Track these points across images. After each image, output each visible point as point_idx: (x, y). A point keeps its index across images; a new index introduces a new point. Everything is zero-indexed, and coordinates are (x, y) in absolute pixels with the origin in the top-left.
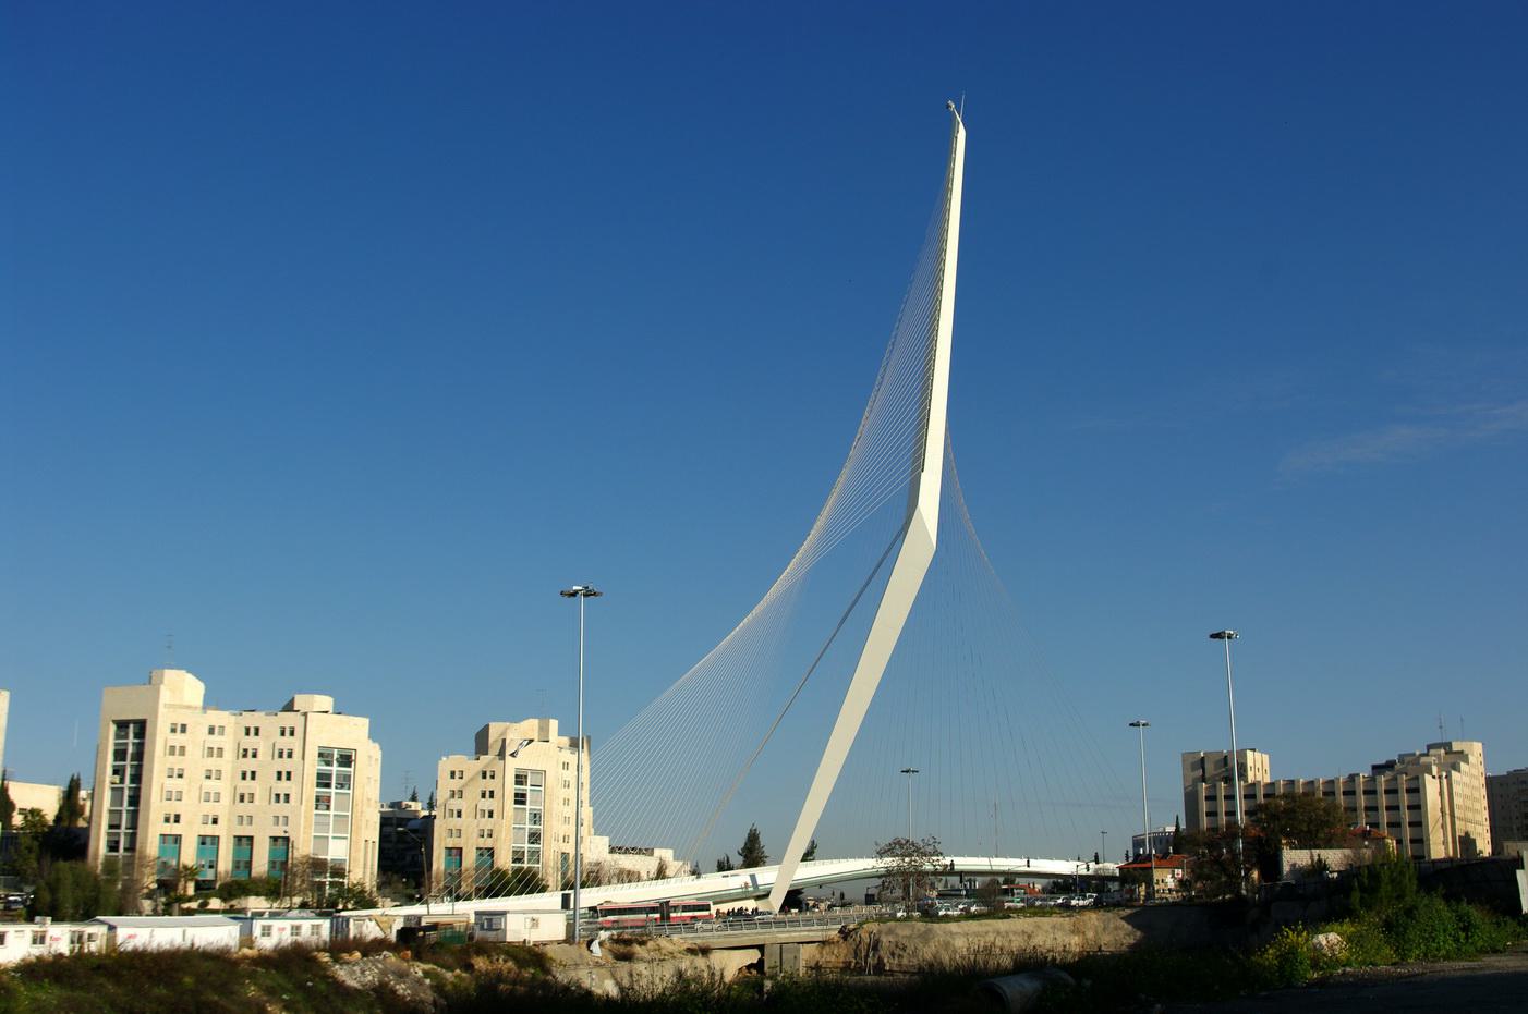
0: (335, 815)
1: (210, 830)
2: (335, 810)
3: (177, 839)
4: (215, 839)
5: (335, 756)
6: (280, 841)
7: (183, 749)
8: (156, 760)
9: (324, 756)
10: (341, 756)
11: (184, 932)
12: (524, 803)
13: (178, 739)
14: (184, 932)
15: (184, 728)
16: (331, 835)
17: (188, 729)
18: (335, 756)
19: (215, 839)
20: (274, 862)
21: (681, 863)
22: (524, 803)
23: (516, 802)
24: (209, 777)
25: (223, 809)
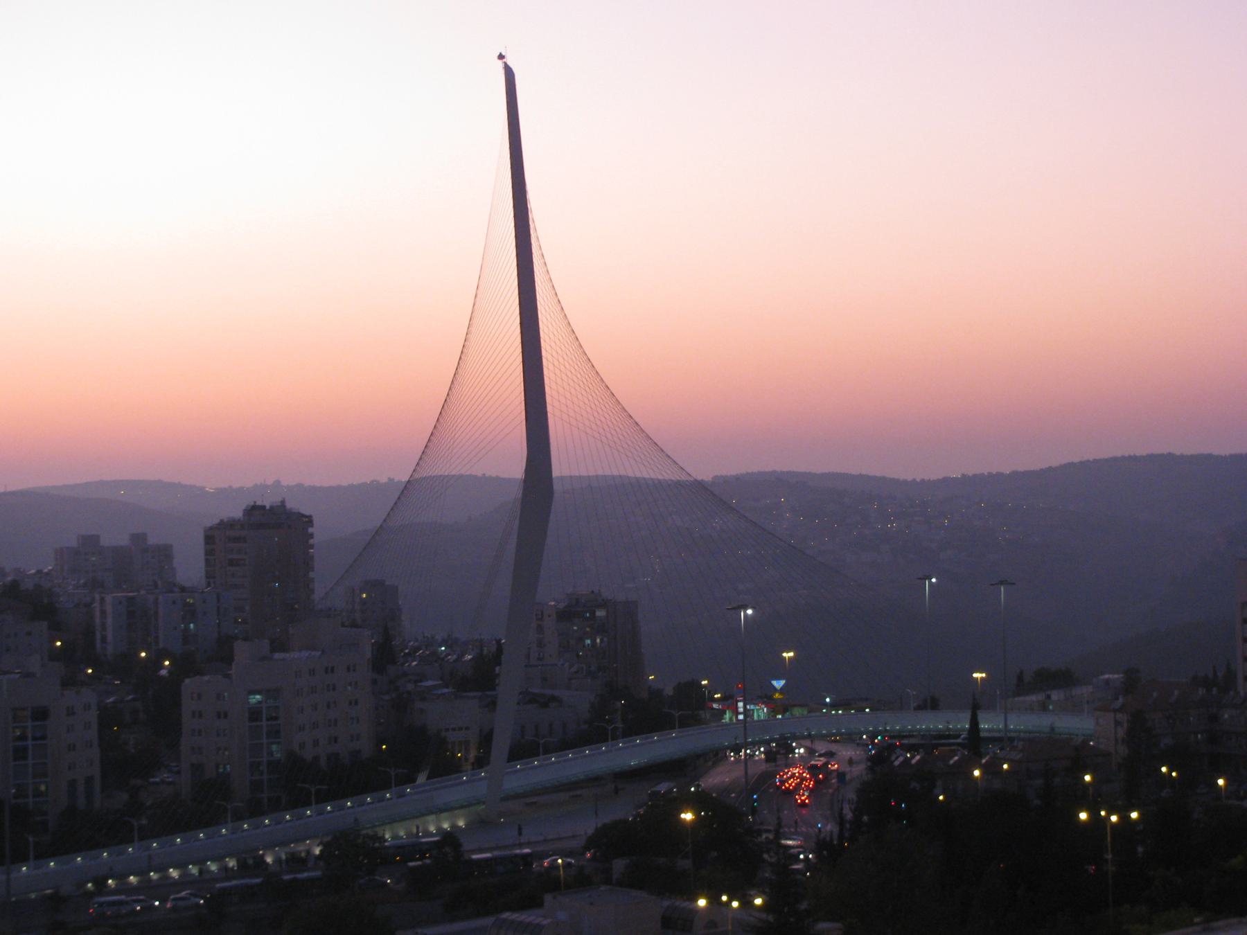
22: (25, 758)
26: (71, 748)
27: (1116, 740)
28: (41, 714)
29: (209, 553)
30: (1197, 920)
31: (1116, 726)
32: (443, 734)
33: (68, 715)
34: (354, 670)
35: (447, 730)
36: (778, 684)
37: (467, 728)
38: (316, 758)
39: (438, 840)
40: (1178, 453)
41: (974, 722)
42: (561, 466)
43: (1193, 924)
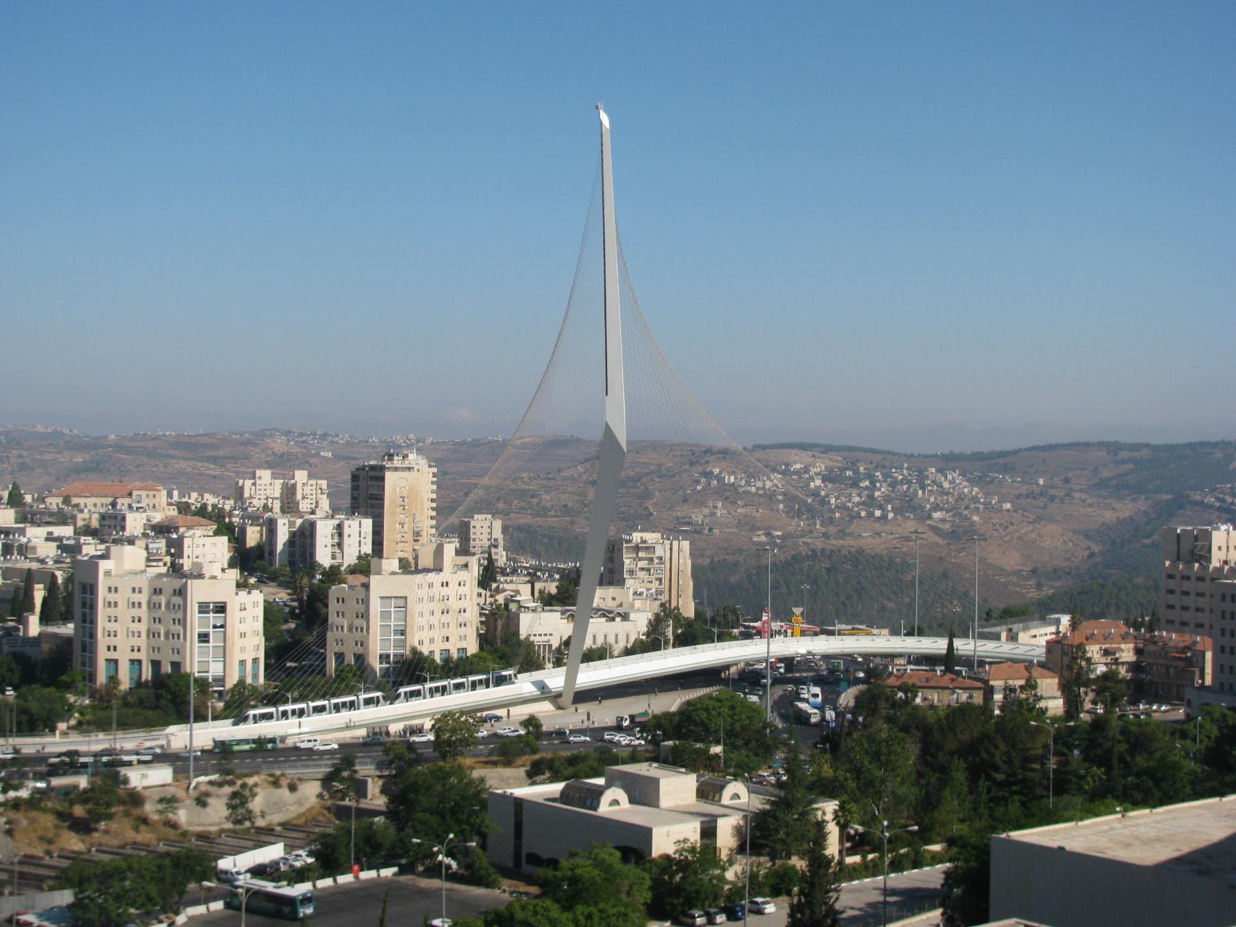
0: (213, 647)
1: (136, 656)
2: (214, 642)
3: (116, 661)
4: (140, 662)
5: (211, 607)
6: (136, 663)
7: (116, 604)
8: (877, 646)
9: (204, 608)
10: (217, 607)
11: (509, 711)
12: (208, 641)
13: (112, 597)
14: (509, 711)
15: (116, 590)
16: (211, 659)
17: (119, 590)
18: (211, 607)
19: (140, 662)
20: (1222, 666)
21: (124, 771)
22: (208, 641)
23: (200, 641)
24: (133, 621)
25: (142, 641)
26: (243, 635)
27: (1062, 665)
28: (221, 608)
29: (355, 488)
30: (1118, 809)
31: (1062, 656)
32: (532, 638)
33: (241, 610)
34: (464, 585)
35: (535, 635)
36: (666, 877)
37: (551, 635)
38: (432, 652)
39: (1052, 613)
40: (1123, 442)
41: (951, 645)
42: (887, 885)
43: (1115, 812)
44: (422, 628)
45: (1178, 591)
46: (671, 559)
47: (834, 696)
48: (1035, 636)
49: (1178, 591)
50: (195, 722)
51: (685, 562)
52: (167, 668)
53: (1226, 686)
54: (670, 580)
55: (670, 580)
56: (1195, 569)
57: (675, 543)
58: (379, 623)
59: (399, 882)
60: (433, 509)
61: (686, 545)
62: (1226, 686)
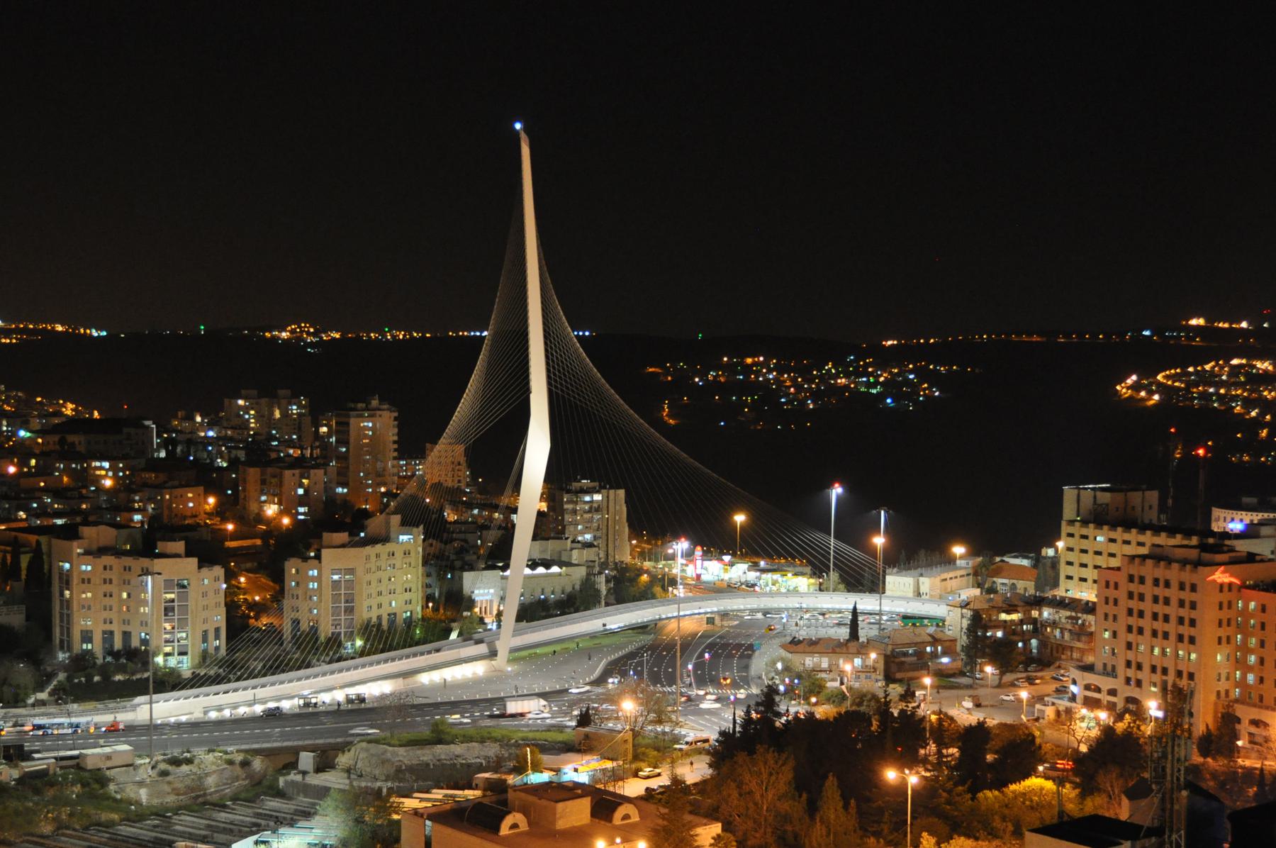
1: (108, 627)
27: (962, 628)
44: (370, 596)
45: (1077, 549)
46: (608, 507)
47: (750, 652)
48: (946, 580)
49: (1077, 549)
50: (155, 692)
51: (621, 508)
52: (135, 643)
53: (1109, 668)
54: (607, 526)
55: (607, 526)
56: (1035, 651)
57: (612, 492)
58: (331, 618)
59: (318, 744)
60: (395, 450)
61: (622, 493)
62: (1109, 668)
